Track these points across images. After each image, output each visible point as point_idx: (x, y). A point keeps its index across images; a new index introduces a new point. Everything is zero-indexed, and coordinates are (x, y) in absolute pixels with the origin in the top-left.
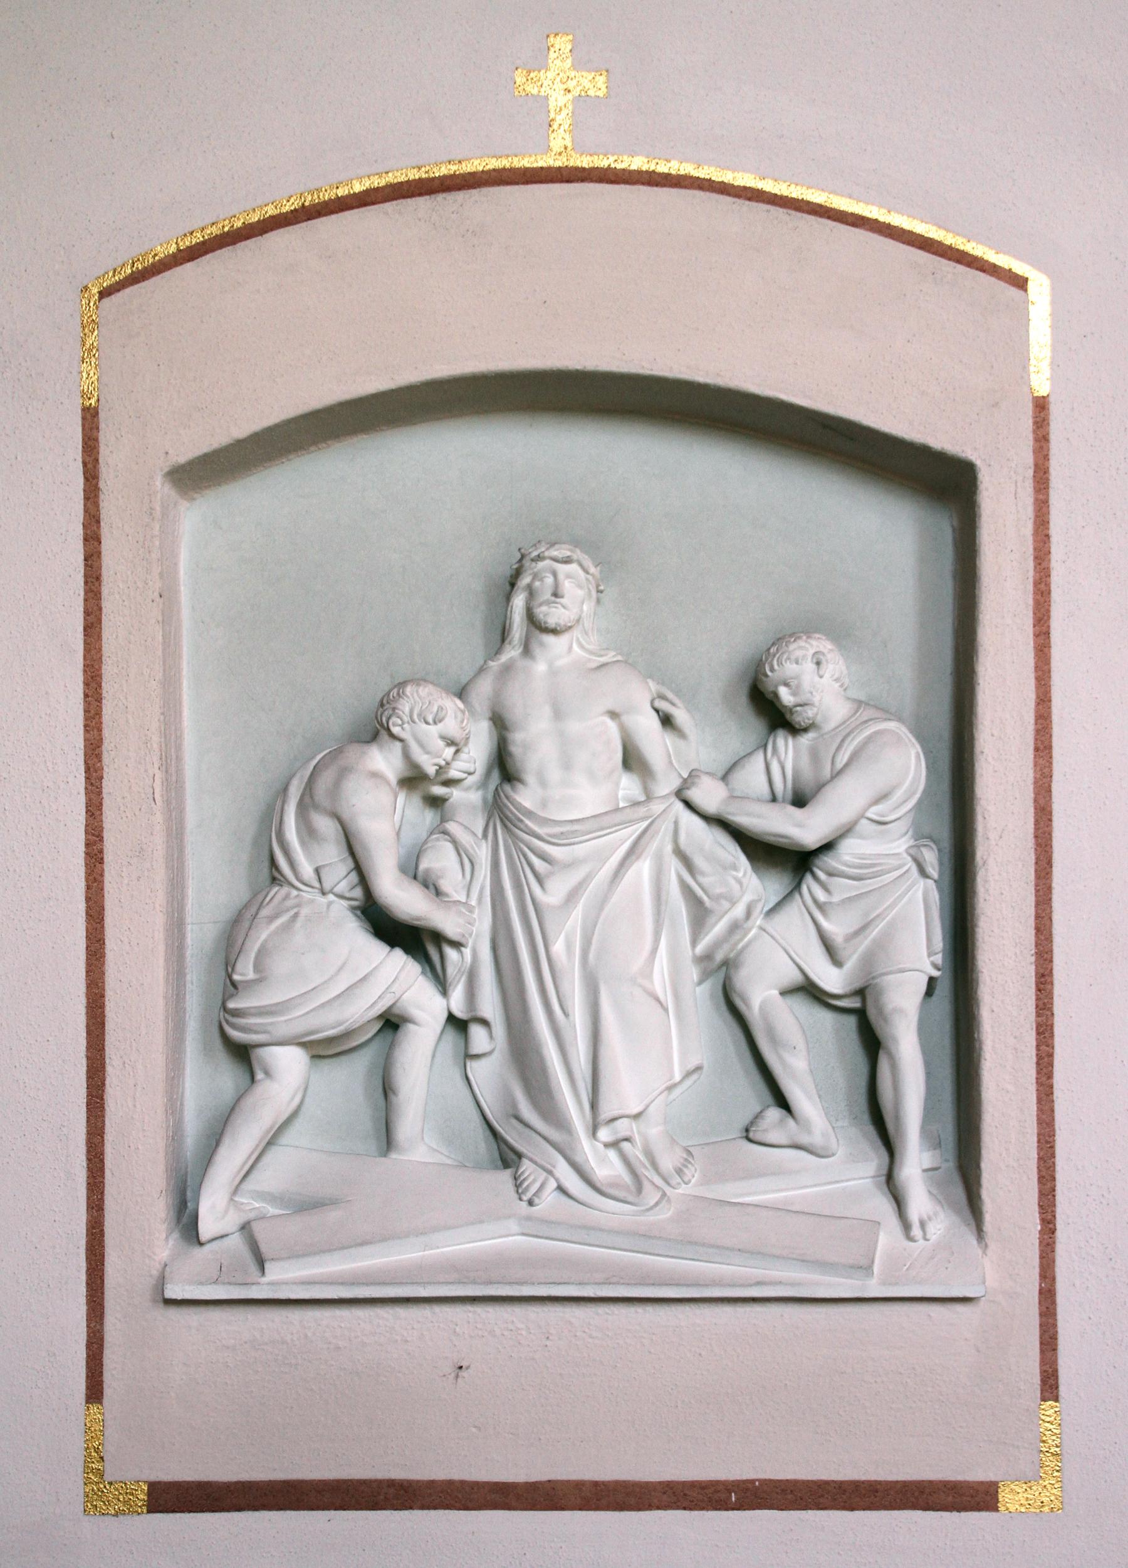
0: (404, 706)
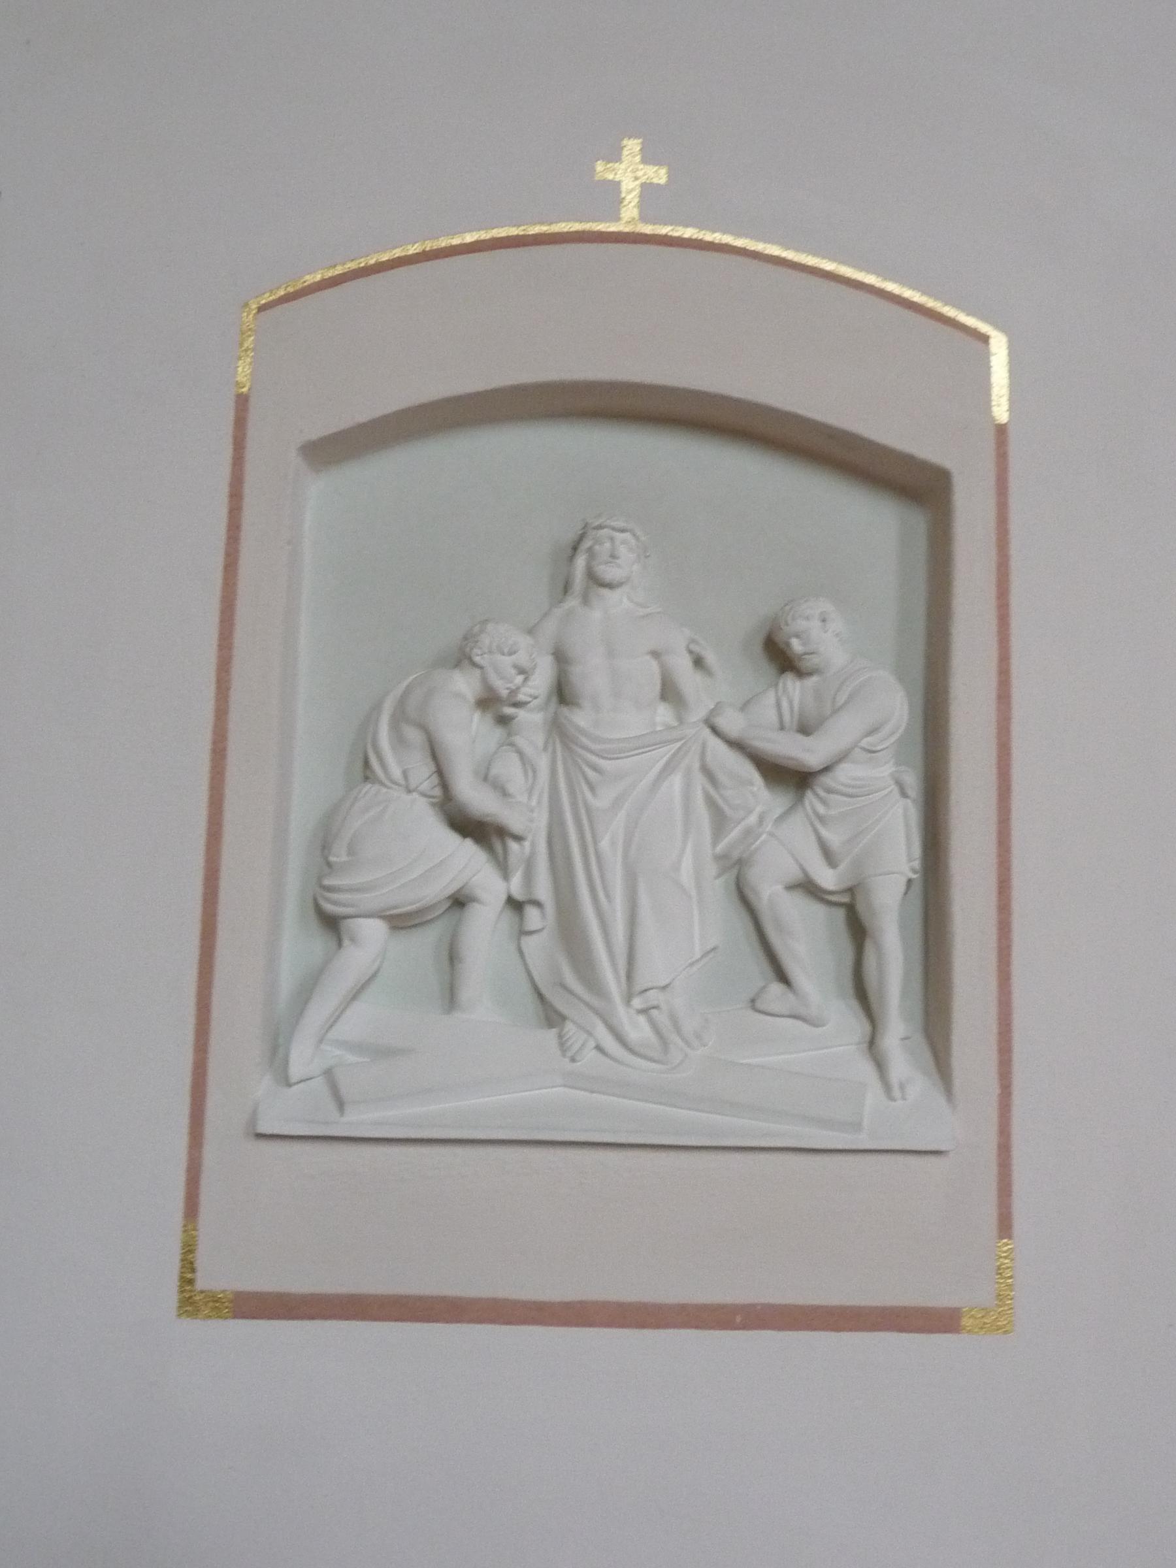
0: (485, 640)
